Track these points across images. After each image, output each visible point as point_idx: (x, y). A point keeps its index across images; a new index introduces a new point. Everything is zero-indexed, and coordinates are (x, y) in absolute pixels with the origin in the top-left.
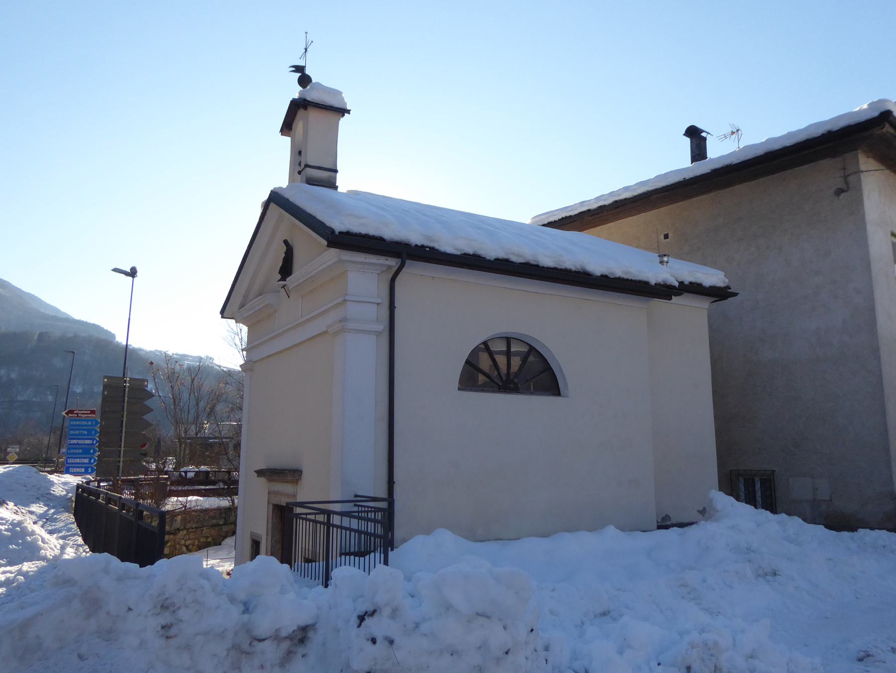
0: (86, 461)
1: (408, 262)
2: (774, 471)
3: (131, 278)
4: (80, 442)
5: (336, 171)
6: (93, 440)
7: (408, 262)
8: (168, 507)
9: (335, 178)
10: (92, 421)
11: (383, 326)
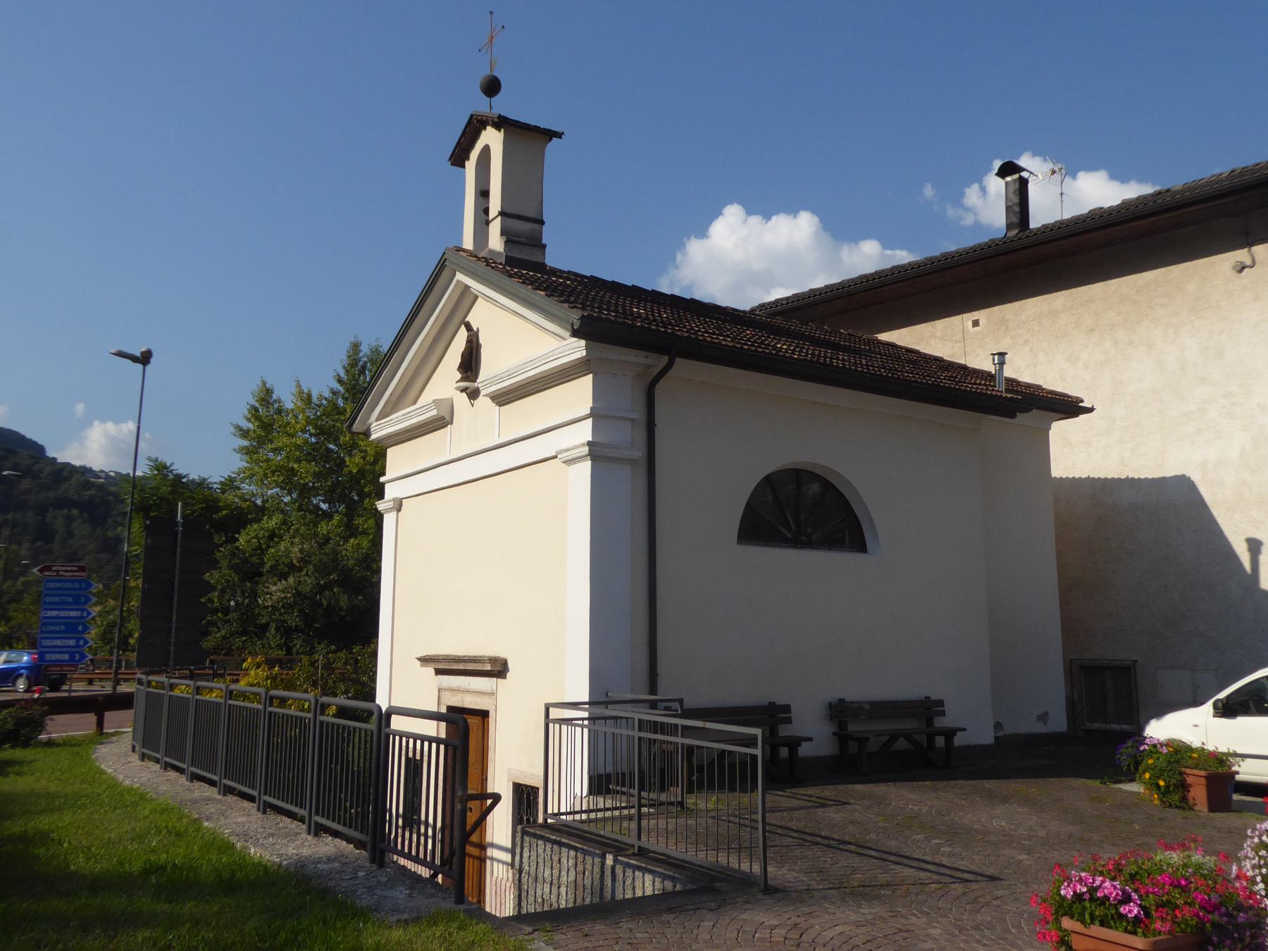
0: (72, 642)
2: (1135, 661)
3: (140, 366)
4: (63, 614)
5: (542, 223)
7: (677, 359)
9: (541, 233)
10: (80, 582)
11: (640, 453)
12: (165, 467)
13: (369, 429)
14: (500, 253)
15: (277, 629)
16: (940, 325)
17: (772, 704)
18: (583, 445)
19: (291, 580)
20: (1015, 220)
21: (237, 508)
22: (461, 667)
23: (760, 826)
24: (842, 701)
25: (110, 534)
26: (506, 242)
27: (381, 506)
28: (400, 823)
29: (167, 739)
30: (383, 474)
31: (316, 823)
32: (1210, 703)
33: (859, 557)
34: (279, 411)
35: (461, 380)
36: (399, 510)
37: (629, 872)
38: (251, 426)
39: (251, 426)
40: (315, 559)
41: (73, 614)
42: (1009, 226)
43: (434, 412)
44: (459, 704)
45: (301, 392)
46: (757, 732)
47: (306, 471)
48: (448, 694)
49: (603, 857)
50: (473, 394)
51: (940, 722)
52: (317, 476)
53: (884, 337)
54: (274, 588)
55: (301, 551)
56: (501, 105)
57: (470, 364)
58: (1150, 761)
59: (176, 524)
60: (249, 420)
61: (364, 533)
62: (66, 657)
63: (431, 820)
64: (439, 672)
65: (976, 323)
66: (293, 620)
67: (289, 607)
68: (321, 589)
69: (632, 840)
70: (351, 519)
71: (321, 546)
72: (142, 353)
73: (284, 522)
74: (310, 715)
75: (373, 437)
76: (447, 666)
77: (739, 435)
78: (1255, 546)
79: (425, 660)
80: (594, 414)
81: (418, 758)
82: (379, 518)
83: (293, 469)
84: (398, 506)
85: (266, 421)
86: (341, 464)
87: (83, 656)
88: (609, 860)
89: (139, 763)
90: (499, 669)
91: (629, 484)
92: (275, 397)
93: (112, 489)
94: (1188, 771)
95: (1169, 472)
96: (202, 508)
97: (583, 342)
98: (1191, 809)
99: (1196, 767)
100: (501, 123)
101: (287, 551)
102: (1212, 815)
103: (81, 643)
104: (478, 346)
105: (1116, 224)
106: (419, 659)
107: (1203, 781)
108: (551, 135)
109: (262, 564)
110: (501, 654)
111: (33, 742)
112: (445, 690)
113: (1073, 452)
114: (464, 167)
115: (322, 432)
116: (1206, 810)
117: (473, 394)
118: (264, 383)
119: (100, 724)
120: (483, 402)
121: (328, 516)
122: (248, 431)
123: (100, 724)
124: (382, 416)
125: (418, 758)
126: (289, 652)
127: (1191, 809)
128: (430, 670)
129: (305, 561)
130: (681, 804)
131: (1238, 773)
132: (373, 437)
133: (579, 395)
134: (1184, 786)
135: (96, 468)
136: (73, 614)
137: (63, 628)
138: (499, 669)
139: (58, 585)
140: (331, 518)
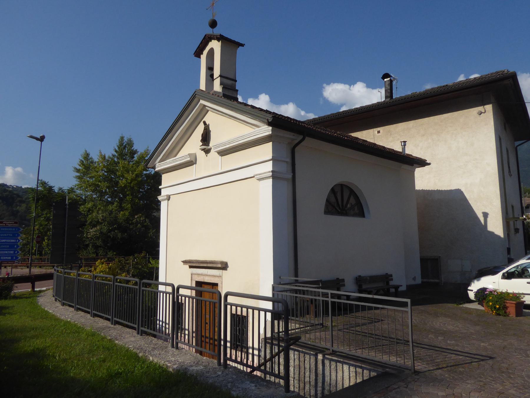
0: (12, 252)
1: (307, 138)
4: (7, 241)
5: (236, 81)
6: (16, 240)
8: (251, 275)
11: (290, 176)
12: (45, 183)
13: (155, 166)
14: (220, 92)
15: (92, 246)
16: (371, 131)
17: (338, 279)
18: (269, 172)
19: (98, 227)
20: (388, 95)
21: (75, 199)
22: (205, 265)
23: (411, 344)
24: (360, 276)
25: (14, 209)
26: (223, 88)
27: (160, 198)
28: (194, 335)
29: (67, 295)
30: (161, 185)
31: (142, 330)
32: (501, 274)
33: (364, 219)
34: (92, 162)
35: (202, 145)
36: (169, 200)
37: (333, 364)
38: (80, 168)
39: (80, 168)
40: (108, 219)
41: (12, 241)
42: (386, 97)
43: (189, 159)
44: (202, 280)
45: (101, 155)
46: (409, 301)
47: (104, 186)
48: (196, 276)
49: (316, 356)
50: (207, 151)
51: (391, 283)
52: (108, 187)
53: (355, 135)
54: (91, 230)
55: (103, 216)
56: (217, 31)
57: (206, 138)
58: (491, 298)
59: (66, 205)
60: (80, 165)
61: (127, 209)
62: (10, 258)
63: (164, 320)
64: (191, 267)
65: (379, 132)
66: (99, 243)
67: (98, 238)
68: (110, 231)
69: (329, 346)
70: (121, 204)
71: (110, 214)
72: (41, 137)
73: (94, 205)
74: (137, 287)
75: (157, 169)
76: (193, 264)
77: (328, 167)
78: (486, 215)
79: (185, 262)
80: (274, 159)
81: (276, 322)
82: (158, 203)
83: (98, 184)
84: (168, 198)
85: (87, 166)
86: (117, 183)
87: (17, 258)
88: (320, 357)
89: (61, 307)
90: (224, 266)
91: (286, 188)
92: (90, 157)
93: (15, 192)
94: (507, 301)
95: (453, 188)
96: (61, 200)
97: (270, 128)
98: (508, 316)
99: (511, 300)
100: (220, 38)
101: (97, 217)
102: (518, 318)
103: (16, 252)
104: (210, 131)
105: (453, 92)
106: (183, 262)
107: (514, 305)
109: (86, 221)
110: (225, 260)
111: (8, 297)
112: (195, 274)
113: (424, 180)
114: (200, 58)
115: (110, 171)
116: (515, 316)
117: (207, 151)
118: (86, 151)
119: (33, 287)
120: (213, 154)
121: (112, 203)
122: (80, 170)
123: (33, 287)
124: (161, 161)
125: (276, 322)
126: (97, 255)
127: (508, 316)
128: (187, 266)
129: (104, 220)
130: (322, 324)
131: (525, 301)
132: (157, 169)
133: (266, 151)
134: (505, 308)
135: (8, 184)
136: (12, 241)
137: (8, 246)
138: (224, 266)
139: (6, 229)
140: (113, 204)
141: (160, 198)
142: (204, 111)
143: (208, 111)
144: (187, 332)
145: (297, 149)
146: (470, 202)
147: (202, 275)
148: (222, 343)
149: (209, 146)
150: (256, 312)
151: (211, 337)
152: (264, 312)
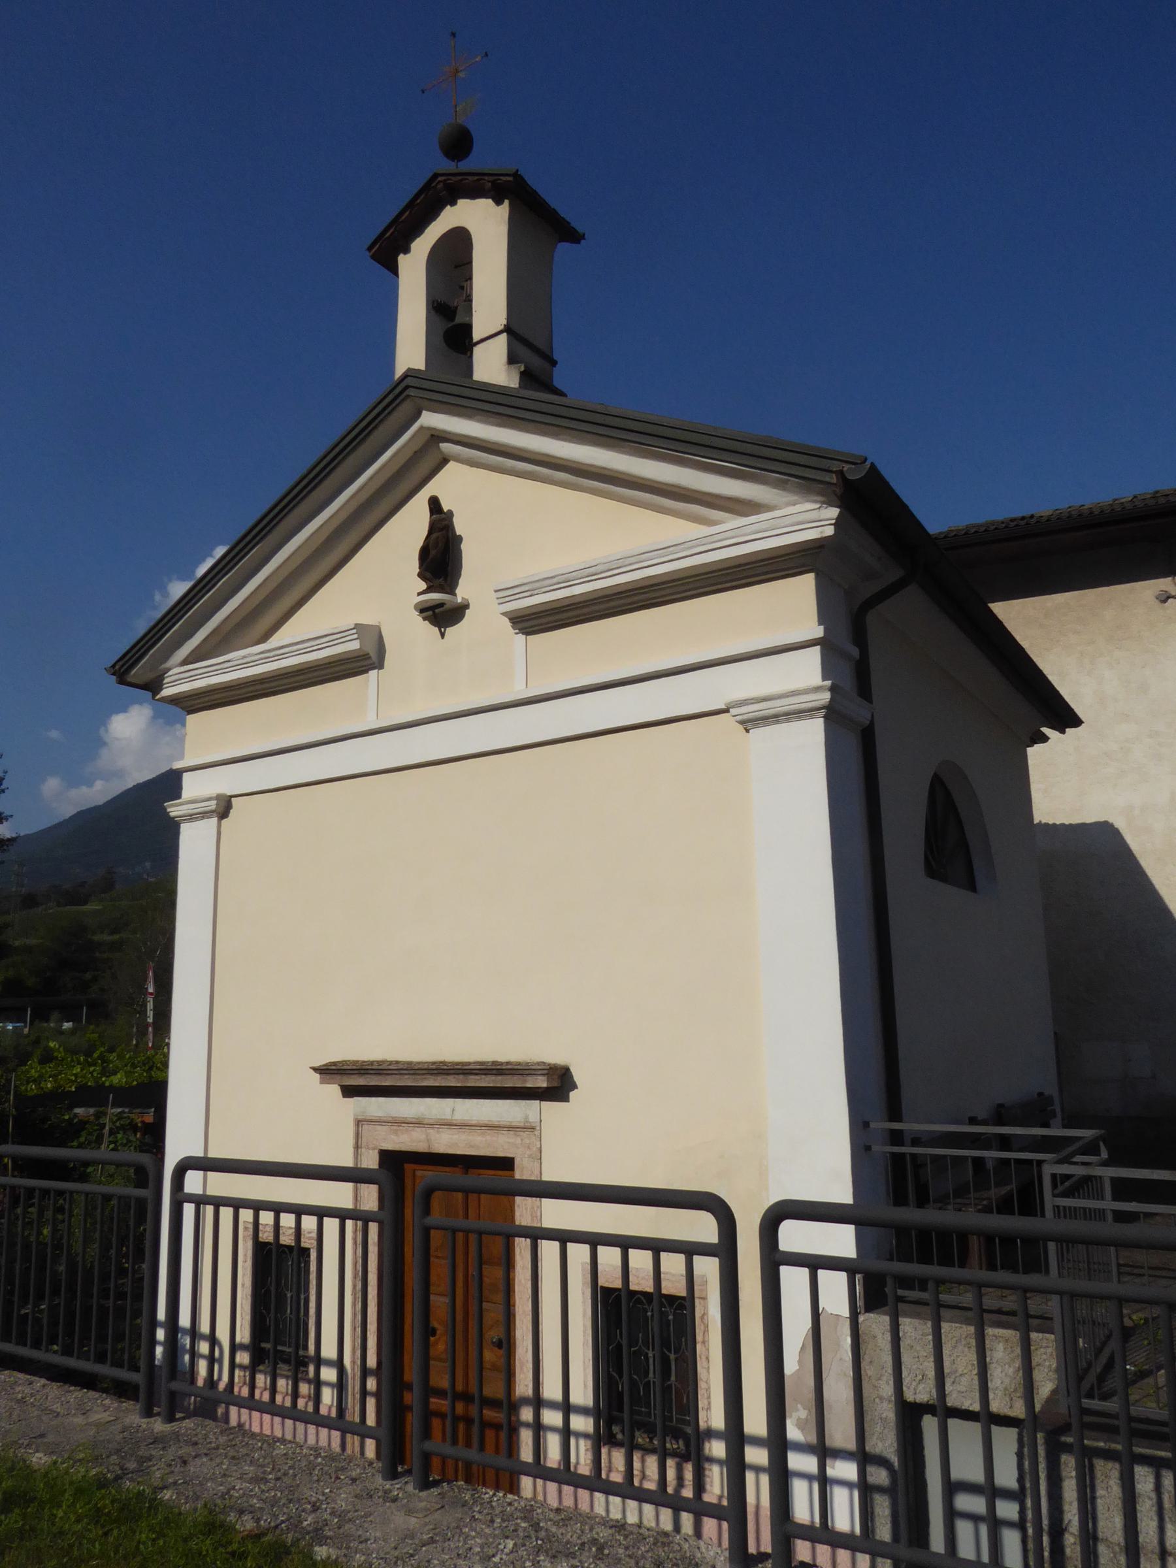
22: (452, 1082)
27: (175, 810)
28: (371, 1384)
30: (182, 757)
43: (355, 645)
48: (382, 1130)
50: (443, 616)
64: (349, 1092)
76: (358, 1080)
79: (328, 1072)
84: (224, 808)
90: (558, 1085)
95: (1090, 818)
108: (573, 236)
112: (370, 1121)
114: (394, 269)
117: (443, 616)
124: (196, 656)
128: (334, 1090)
138: (558, 1085)
141: (175, 810)
142: (431, 455)
143: (445, 461)
144: (329, 1374)
145: (871, 618)
146: (1144, 863)
147: (419, 1123)
148: (160, 1334)
149: (452, 592)
150: (226, 1213)
151: (460, 1387)
152: (231, 1210)
